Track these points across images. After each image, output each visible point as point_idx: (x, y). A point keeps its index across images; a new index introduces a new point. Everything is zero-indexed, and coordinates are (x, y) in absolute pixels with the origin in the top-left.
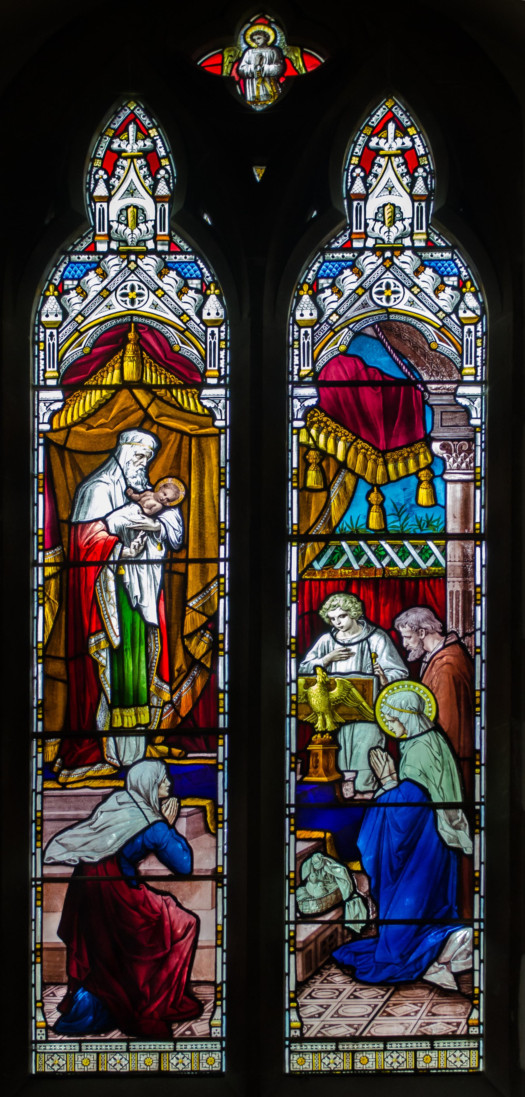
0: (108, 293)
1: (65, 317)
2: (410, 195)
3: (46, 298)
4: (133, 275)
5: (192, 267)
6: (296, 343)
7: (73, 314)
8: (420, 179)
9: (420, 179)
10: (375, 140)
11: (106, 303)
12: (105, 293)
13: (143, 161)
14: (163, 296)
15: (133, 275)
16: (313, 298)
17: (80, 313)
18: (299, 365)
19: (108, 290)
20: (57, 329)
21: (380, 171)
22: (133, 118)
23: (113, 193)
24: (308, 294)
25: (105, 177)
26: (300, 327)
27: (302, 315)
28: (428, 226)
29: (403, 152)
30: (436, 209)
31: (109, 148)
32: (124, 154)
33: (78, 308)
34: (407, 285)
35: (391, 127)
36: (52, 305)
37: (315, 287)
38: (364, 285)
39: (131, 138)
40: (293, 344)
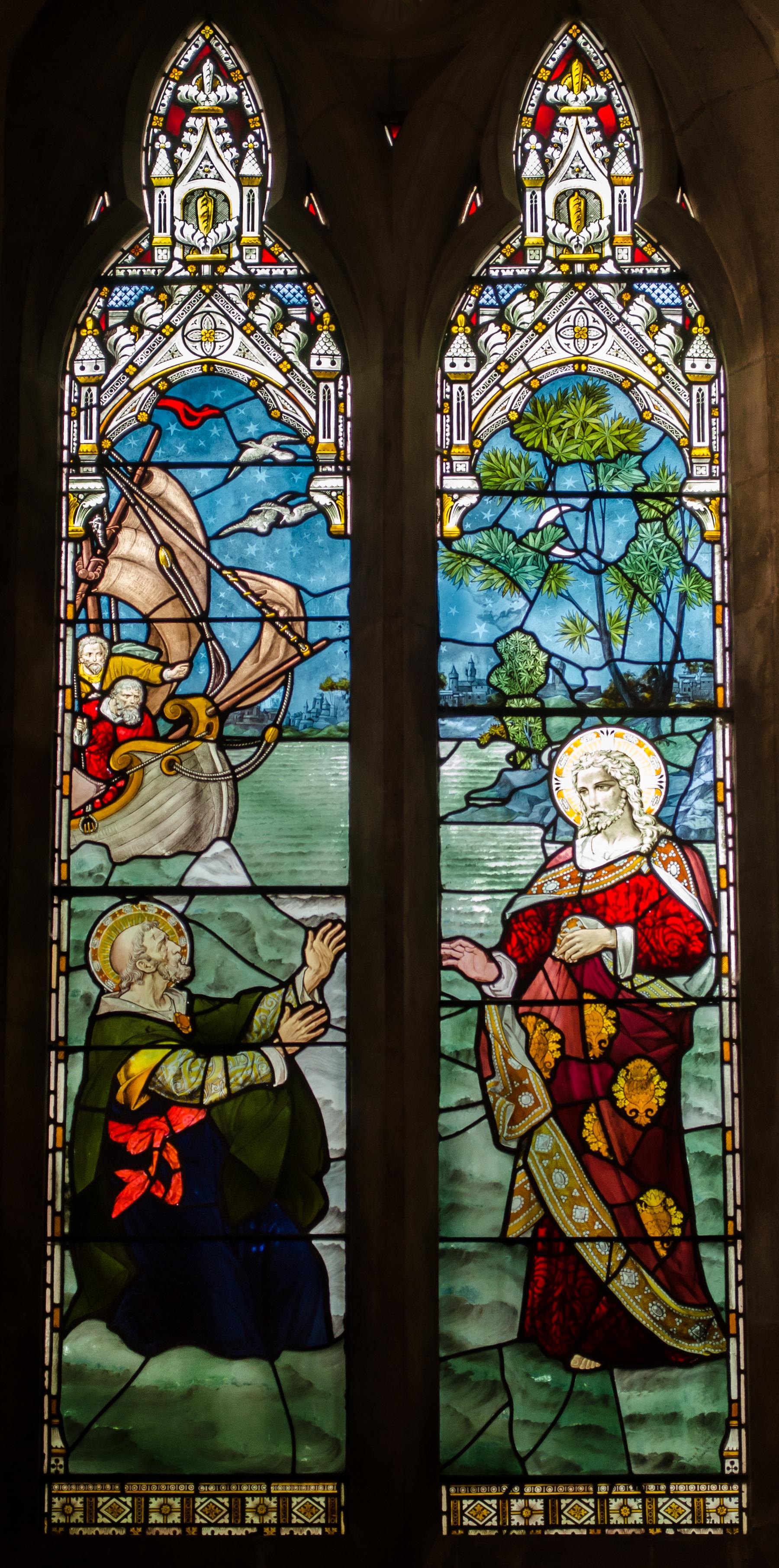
0: (544, 327)
1: (479, 366)
2: (609, 177)
3: (81, 340)
4: (208, 302)
5: (125, 292)
6: (446, 405)
7: (494, 359)
8: (163, 152)
9: (163, 152)
10: (553, 89)
11: (167, 348)
12: (539, 327)
13: (593, 122)
14: (253, 333)
15: (208, 302)
16: (473, 339)
17: (503, 359)
18: (451, 437)
19: (171, 325)
20: (469, 382)
21: (565, 140)
22: (574, 52)
23: (550, 173)
24: (328, 330)
25: (168, 145)
26: (80, 385)
27: (453, 365)
28: (633, 227)
29: (597, 108)
30: (275, 202)
31: (174, 99)
32: (564, 109)
33: (501, 350)
34: (237, 321)
35: (208, 67)
36: (90, 348)
37: (473, 320)
38: (545, 317)
39: (207, 80)
40: (443, 407)
